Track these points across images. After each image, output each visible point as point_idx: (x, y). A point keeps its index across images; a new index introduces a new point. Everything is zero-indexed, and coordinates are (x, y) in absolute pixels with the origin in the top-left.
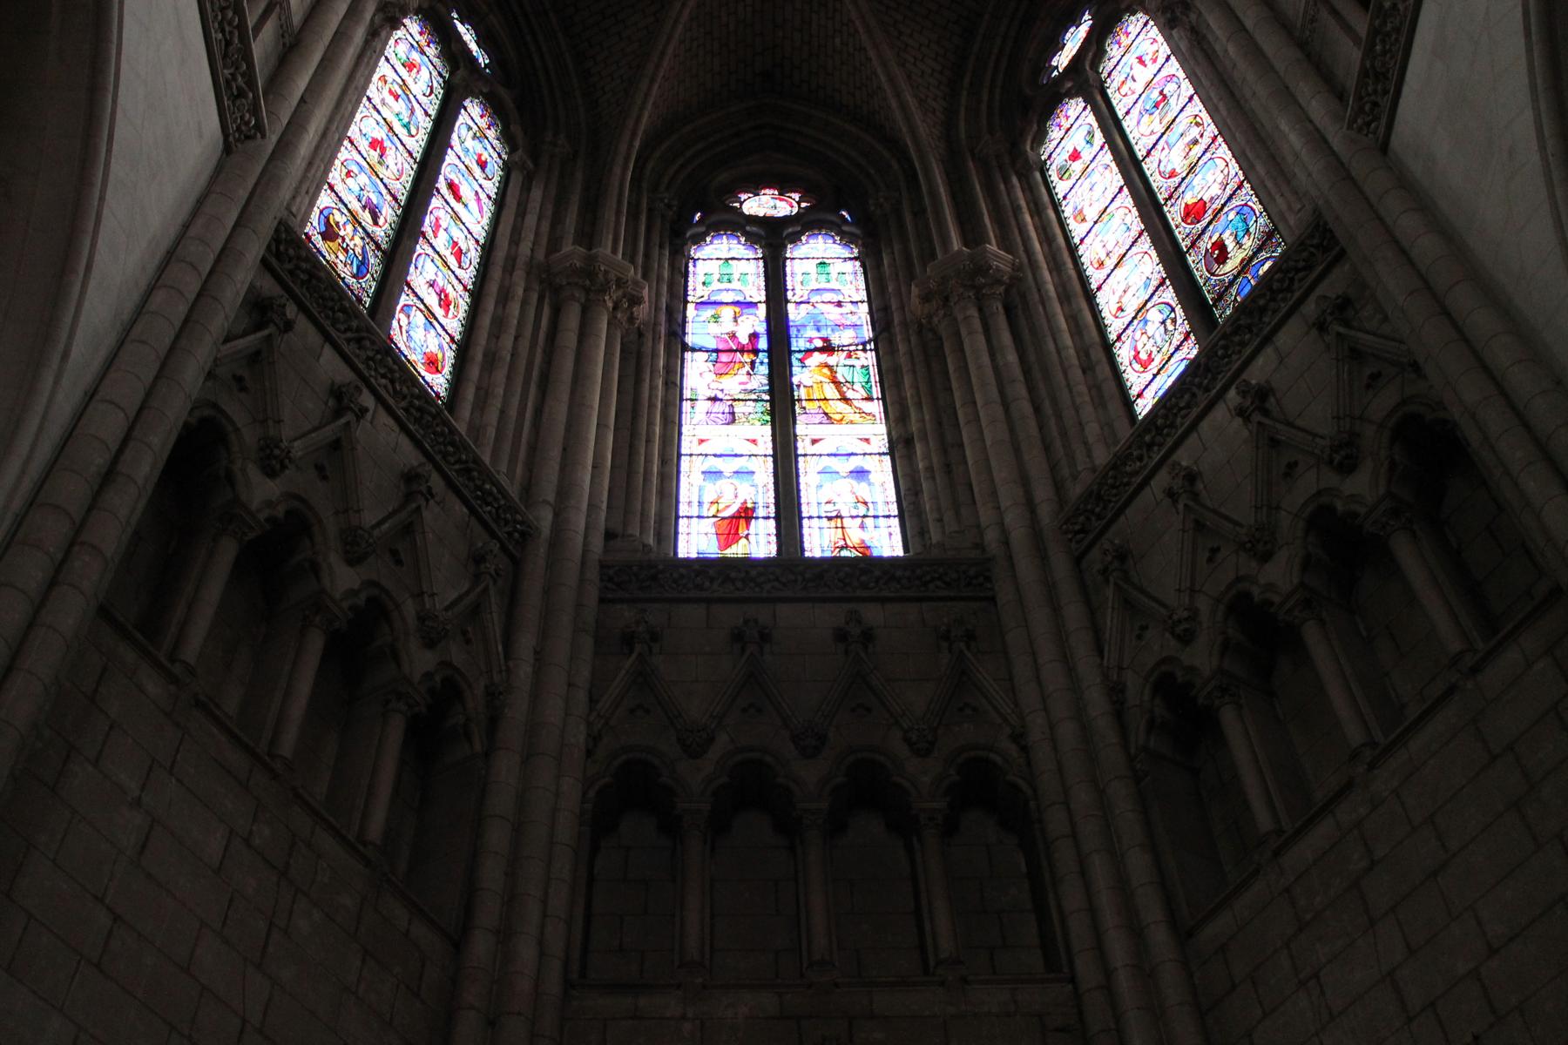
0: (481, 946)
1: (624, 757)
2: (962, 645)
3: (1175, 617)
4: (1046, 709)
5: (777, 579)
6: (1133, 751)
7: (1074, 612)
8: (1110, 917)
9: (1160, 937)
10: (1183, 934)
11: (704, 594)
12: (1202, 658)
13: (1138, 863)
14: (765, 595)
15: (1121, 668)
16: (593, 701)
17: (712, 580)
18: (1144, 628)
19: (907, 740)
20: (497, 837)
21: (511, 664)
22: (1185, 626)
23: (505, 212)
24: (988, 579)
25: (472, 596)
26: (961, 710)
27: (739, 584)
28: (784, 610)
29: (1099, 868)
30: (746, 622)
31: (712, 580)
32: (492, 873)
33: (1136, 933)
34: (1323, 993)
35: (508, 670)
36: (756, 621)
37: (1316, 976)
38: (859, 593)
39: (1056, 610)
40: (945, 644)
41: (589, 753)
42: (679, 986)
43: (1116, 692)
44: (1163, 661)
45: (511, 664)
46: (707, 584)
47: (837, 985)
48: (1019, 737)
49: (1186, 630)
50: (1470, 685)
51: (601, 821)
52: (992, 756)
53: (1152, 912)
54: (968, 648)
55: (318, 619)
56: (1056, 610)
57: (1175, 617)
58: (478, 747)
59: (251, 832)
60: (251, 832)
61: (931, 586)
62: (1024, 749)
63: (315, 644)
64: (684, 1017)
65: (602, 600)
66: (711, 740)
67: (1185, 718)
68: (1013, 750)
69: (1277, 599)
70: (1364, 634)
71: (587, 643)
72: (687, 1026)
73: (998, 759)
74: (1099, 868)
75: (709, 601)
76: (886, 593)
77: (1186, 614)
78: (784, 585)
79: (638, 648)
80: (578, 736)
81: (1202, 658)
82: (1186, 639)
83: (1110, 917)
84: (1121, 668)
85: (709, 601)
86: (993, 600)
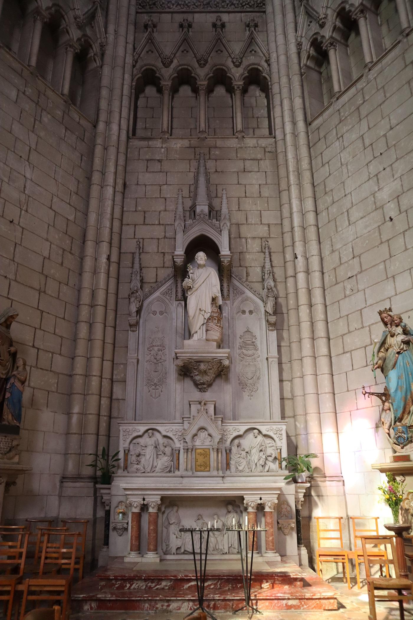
0: (101, 126)
1: (145, 68)
2: (253, 29)
3: (320, 17)
4: (277, 52)
5: (194, 4)
6: (302, 65)
7: (290, 16)
8: (287, 119)
9: (301, 125)
10: (308, 124)
11: (171, 10)
12: (327, 33)
13: (298, 102)
14: (190, 10)
15: (301, 37)
16: (134, 49)
17: (173, 5)
18: (311, 22)
19: (233, 62)
20: (104, 92)
21: (107, 35)
22: (323, 20)
23: (304, 87)
24: (264, 4)
25: (92, 10)
26: (251, 52)
27: (182, 6)
28: (196, 16)
29: (286, 103)
30: (184, 20)
31: (173, 5)
32: (103, 104)
33: (294, 123)
34: (343, 141)
35: (106, 38)
36: (187, 20)
37: (342, 136)
38: (222, 9)
39: (284, 15)
40: (247, 29)
41: (134, 66)
42: (161, 138)
43: (299, 45)
44: (315, 34)
45: (107, 35)
46: (172, 6)
47: (206, 138)
48: (267, 61)
49: (323, 22)
50: (405, 40)
51: (138, 90)
52: (259, 67)
53: (300, 117)
54: (255, 30)
55: (39, 17)
56: (284, 15)
57: (320, 17)
58: (98, 64)
59: (25, 91)
60: (25, 91)
61: (245, 7)
62: (269, 65)
63: (39, 26)
64: (162, 147)
65: (137, 13)
66: (172, 62)
67: (320, 56)
68: (265, 65)
69: (353, 9)
70: (380, 23)
71: (131, 28)
72: (163, 150)
73: (261, 68)
74: (286, 103)
75: (172, 13)
76: (230, 10)
77: (324, 16)
78: (197, 6)
79: (149, 30)
80: (129, 60)
81: (327, 33)
82: (322, 26)
83: (287, 119)
84: (301, 37)
85: (172, 13)
86: (265, 12)
